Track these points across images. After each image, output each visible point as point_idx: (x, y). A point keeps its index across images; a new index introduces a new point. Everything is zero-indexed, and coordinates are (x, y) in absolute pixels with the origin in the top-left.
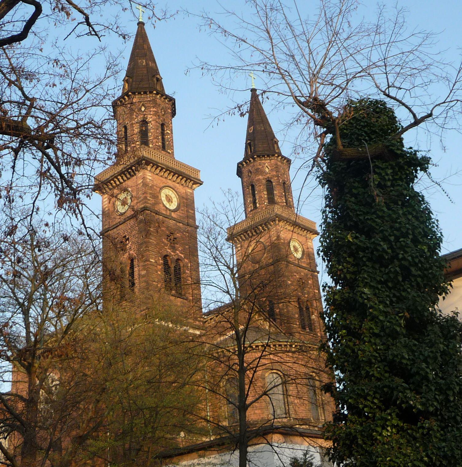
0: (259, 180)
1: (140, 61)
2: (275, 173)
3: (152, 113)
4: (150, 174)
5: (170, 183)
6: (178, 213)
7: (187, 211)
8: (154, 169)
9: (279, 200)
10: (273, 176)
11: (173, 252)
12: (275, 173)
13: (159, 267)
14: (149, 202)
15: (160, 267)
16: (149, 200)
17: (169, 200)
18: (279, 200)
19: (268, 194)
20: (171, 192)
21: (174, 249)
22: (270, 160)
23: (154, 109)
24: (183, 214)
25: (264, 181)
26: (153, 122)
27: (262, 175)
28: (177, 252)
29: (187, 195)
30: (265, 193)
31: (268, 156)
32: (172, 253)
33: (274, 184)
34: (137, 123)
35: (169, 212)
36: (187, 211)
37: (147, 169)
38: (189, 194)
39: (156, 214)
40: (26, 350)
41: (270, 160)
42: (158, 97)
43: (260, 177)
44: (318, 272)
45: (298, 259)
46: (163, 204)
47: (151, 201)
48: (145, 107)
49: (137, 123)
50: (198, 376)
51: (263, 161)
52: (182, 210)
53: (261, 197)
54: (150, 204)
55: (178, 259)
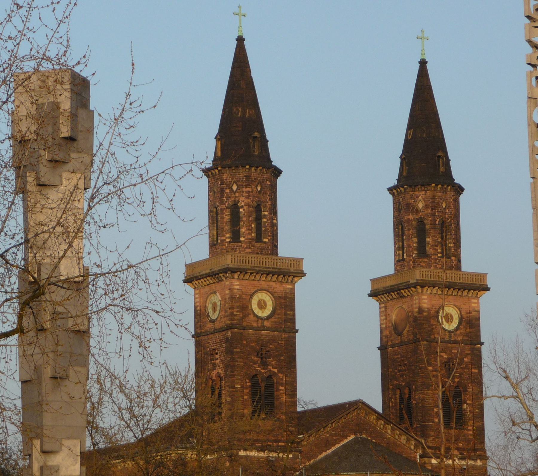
0: (409, 221)
1: (235, 109)
2: (429, 211)
3: (244, 194)
4: (238, 283)
5: (264, 284)
6: (273, 319)
7: (285, 314)
8: (242, 276)
9: (432, 251)
10: (427, 215)
11: (263, 369)
12: (429, 211)
13: (246, 391)
14: (236, 317)
15: (248, 391)
16: (236, 315)
17: (262, 305)
18: (431, 250)
19: (418, 243)
20: (265, 295)
21: (264, 365)
22: (426, 191)
23: (248, 189)
24: (279, 318)
25: (414, 223)
26: (245, 208)
27: (412, 213)
28: (269, 367)
29: (286, 293)
30: (415, 240)
31: (422, 185)
32: (263, 371)
33: (427, 227)
34: (227, 208)
35: (260, 321)
36: (285, 314)
37: (234, 278)
38: (288, 291)
39: (244, 329)
40: (20, 193)
41: (426, 191)
42: (253, 169)
43: (411, 217)
44: (482, 344)
45: (450, 332)
46: (254, 314)
47: (238, 314)
48: (237, 185)
49: (227, 208)
50: (404, 437)
51: (416, 193)
52: (278, 314)
53: (409, 246)
54: (237, 319)
55: (270, 376)
